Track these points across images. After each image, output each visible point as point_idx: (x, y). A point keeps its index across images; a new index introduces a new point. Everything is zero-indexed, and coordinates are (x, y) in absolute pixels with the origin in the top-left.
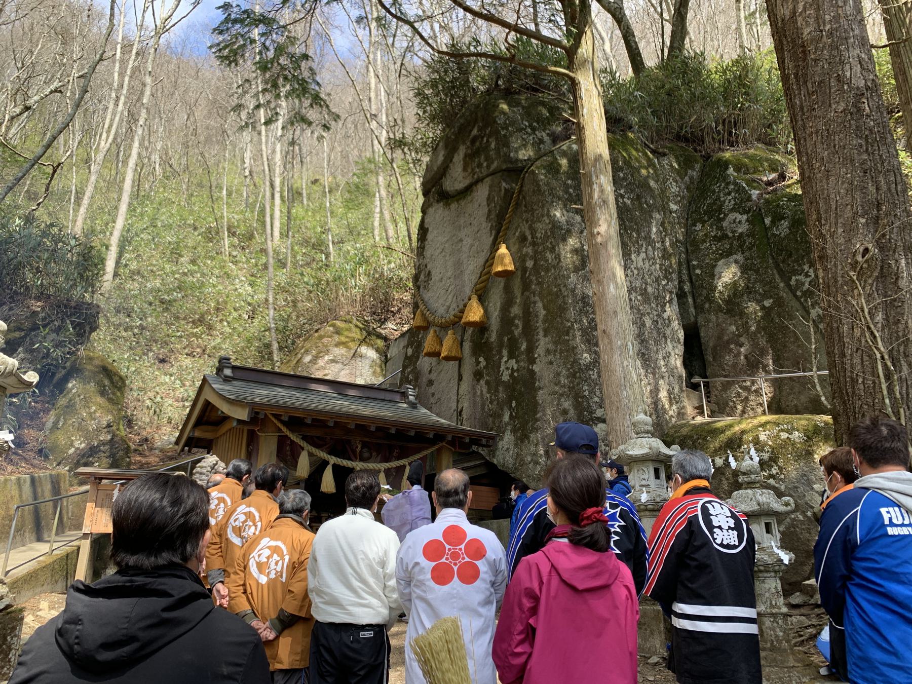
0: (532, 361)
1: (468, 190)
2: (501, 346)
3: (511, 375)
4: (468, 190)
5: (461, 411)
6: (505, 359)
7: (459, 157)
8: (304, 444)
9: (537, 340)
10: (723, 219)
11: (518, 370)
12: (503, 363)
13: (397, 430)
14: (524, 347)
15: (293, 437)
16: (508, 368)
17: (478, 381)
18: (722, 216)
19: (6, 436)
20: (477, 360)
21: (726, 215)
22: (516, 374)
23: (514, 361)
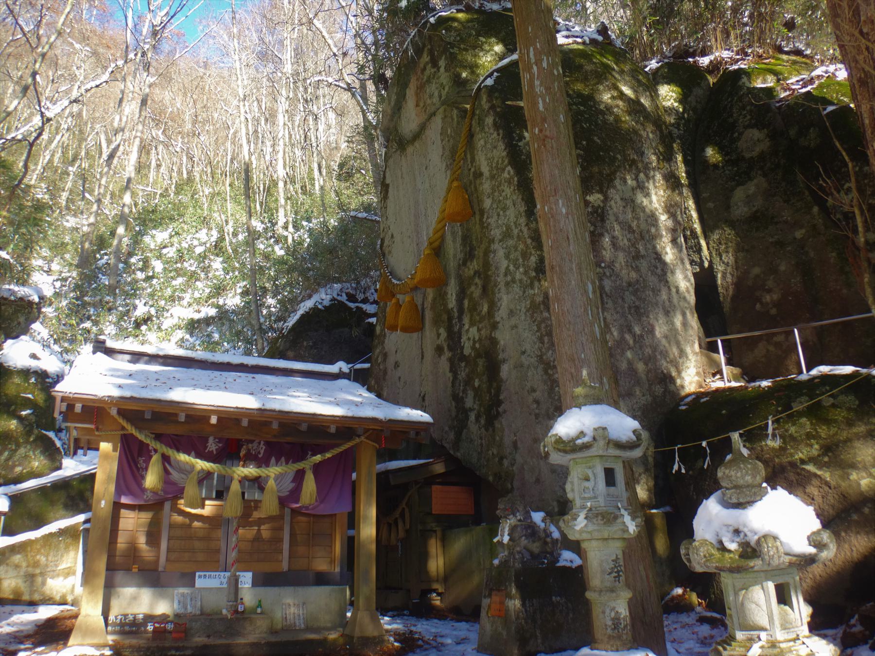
0: (494, 326)
1: (423, 127)
2: (461, 311)
3: (473, 347)
4: (423, 127)
5: (424, 396)
6: (466, 327)
7: (410, 92)
8: (153, 444)
9: (499, 300)
10: (739, 139)
11: (480, 340)
12: (463, 333)
13: (250, 422)
14: (485, 309)
15: (141, 437)
16: (469, 339)
17: (440, 356)
18: (736, 134)
19: (404, 4)
20: (437, 331)
21: (741, 134)
22: (477, 345)
23: (475, 328)
